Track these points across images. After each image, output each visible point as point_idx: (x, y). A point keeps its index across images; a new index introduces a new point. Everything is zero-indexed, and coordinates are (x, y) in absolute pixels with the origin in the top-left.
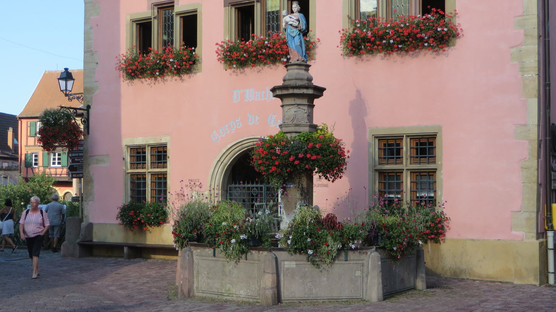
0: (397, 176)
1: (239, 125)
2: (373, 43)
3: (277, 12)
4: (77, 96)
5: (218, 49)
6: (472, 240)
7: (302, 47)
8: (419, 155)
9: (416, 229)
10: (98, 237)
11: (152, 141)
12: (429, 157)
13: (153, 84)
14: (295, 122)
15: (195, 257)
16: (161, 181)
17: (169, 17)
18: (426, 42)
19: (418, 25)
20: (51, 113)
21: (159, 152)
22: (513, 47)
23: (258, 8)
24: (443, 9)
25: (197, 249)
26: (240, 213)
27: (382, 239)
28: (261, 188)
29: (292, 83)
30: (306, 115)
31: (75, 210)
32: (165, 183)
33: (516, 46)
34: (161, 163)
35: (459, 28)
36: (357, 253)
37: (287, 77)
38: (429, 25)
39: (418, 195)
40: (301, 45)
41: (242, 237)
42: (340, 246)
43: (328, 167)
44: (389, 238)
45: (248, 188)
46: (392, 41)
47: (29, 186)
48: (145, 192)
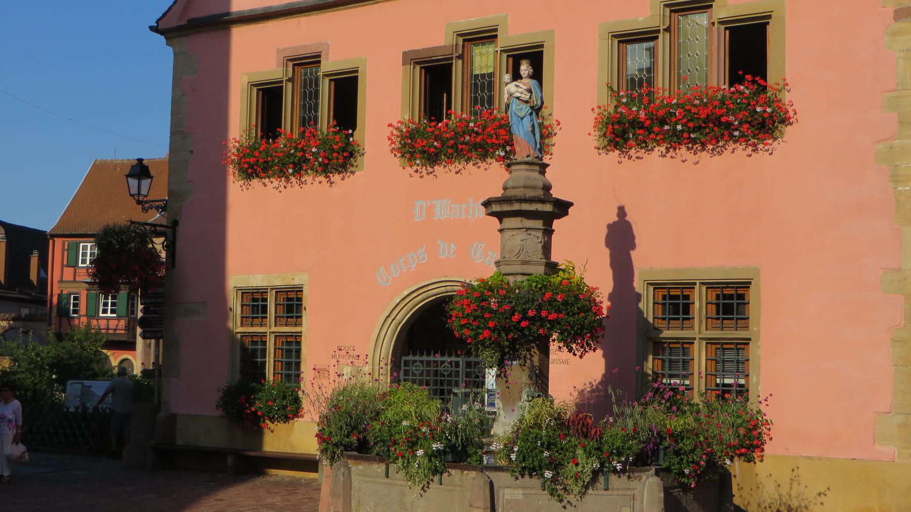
0: (684, 348)
1: (423, 258)
2: (649, 130)
3: (491, 75)
4: (157, 204)
5: (392, 133)
6: (809, 458)
7: (534, 135)
8: (721, 316)
9: (721, 439)
10: (184, 437)
11: (279, 281)
12: (738, 319)
13: (282, 188)
14: (522, 257)
15: (354, 478)
16: (291, 349)
17: (311, 80)
18: (736, 130)
19: (722, 102)
20: (114, 231)
21: (289, 299)
22: (879, 142)
23: (457, 68)
24: (764, 77)
25: (358, 464)
26: (432, 409)
27: (665, 455)
28: (457, 364)
29: (519, 193)
30: (540, 246)
31: (144, 392)
32: (298, 352)
33: (883, 140)
34: (292, 317)
35: (790, 109)
36: (624, 478)
37: (510, 184)
38: (740, 103)
39: (718, 381)
40: (533, 132)
41: (435, 446)
42: (596, 465)
43: (576, 332)
44: (677, 453)
45: (429, 363)
46: (679, 127)
47: (64, 348)
48: (264, 364)
